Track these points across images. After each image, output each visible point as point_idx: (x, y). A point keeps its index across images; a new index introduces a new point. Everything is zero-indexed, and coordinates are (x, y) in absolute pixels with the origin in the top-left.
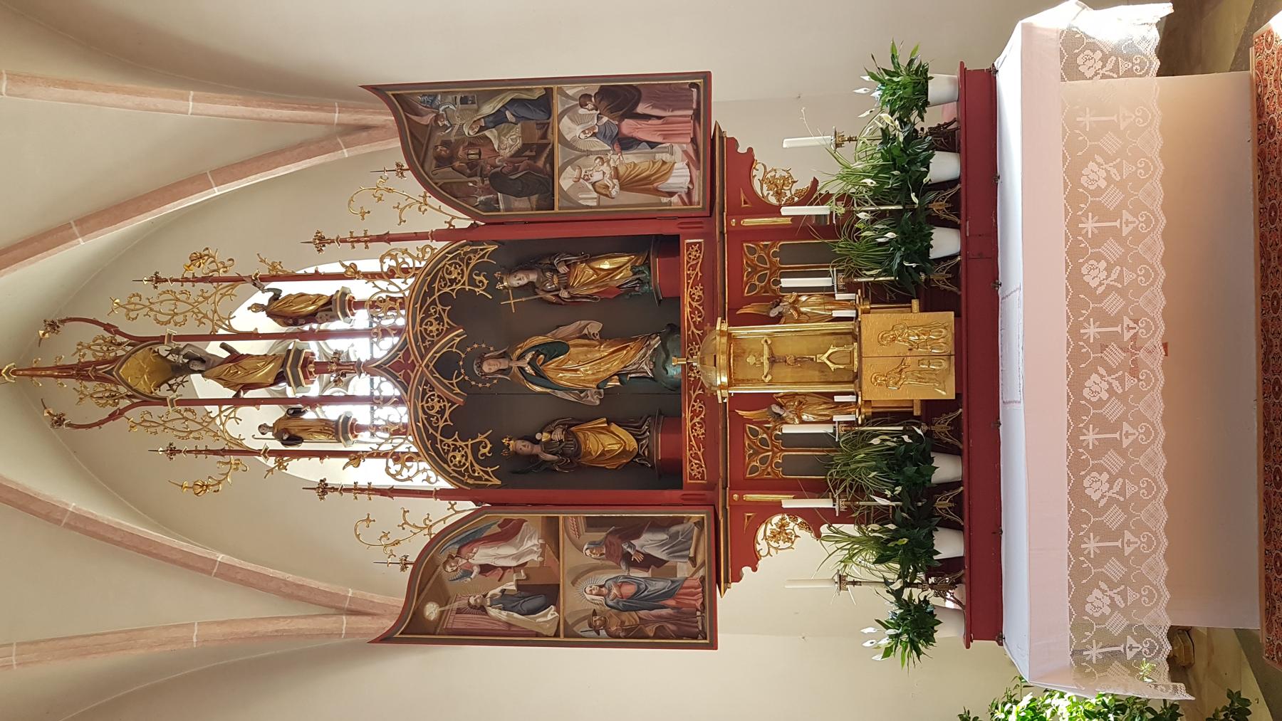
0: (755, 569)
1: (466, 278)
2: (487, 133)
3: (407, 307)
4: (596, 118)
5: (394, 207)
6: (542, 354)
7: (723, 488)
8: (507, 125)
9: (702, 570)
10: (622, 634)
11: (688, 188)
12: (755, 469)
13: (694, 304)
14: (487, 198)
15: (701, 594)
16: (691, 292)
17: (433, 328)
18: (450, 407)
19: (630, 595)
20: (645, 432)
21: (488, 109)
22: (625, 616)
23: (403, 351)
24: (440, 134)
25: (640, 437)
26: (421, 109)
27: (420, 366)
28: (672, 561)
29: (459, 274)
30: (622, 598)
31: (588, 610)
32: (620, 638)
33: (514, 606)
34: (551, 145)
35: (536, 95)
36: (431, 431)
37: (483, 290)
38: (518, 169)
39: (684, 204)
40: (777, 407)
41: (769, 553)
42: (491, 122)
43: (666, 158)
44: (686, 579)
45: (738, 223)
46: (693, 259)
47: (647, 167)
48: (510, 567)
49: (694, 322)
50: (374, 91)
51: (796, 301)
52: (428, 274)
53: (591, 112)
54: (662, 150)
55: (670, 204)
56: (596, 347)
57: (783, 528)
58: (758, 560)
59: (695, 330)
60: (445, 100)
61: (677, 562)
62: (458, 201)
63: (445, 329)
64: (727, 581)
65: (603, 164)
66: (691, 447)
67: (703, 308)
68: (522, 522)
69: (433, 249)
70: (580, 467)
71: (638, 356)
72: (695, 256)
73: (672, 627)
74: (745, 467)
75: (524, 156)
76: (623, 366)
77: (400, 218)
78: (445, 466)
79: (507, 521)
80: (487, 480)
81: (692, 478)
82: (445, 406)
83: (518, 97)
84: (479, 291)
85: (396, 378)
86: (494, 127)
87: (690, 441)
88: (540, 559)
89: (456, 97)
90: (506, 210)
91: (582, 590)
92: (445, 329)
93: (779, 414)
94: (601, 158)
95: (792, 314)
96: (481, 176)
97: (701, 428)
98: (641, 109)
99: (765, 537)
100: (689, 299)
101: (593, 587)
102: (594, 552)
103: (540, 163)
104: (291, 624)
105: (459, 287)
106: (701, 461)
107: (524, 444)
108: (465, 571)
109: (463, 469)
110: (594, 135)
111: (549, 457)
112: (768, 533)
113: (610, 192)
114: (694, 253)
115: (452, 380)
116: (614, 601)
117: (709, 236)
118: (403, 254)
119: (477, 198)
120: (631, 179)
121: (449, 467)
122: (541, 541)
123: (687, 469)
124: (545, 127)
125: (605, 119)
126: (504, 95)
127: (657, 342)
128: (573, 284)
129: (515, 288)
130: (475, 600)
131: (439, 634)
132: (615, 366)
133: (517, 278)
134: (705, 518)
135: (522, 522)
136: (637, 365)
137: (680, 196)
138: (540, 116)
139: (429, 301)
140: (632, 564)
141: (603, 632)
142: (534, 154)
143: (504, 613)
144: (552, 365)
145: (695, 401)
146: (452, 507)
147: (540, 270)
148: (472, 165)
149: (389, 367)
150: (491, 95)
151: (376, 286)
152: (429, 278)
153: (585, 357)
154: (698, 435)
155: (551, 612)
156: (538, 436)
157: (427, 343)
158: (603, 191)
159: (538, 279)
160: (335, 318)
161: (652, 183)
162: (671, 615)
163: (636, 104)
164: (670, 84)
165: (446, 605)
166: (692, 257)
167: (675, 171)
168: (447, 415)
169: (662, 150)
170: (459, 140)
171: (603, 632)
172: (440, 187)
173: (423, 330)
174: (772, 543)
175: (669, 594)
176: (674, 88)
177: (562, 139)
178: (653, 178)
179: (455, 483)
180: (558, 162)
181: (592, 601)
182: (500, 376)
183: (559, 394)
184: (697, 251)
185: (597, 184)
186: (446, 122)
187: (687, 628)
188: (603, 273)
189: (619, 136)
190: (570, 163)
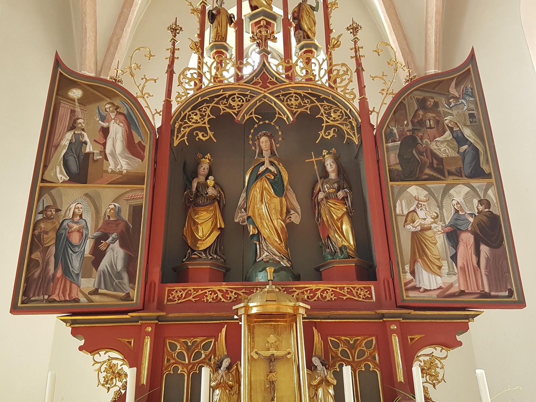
0: (81, 348)
1: (331, 123)
2: (448, 132)
3: (307, 82)
4: (471, 212)
5: (383, 73)
6: (275, 178)
7: (159, 316)
8: (457, 146)
9: (86, 300)
10: (36, 232)
11: (420, 288)
12: (173, 347)
13: (319, 293)
14: (395, 134)
15: (63, 299)
16: (329, 290)
17: (293, 102)
18: (234, 113)
19: (70, 240)
20: (211, 256)
21: (467, 133)
22: (53, 235)
23: (276, 81)
24: (443, 100)
25: (207, 252)
26: (461, 87)
27: (265, 92)
28: (96, 274)
29: (334, 118)
30: (68, 233)
31: (62, 205)
32: (34, 229)
33: (72, 150)
34: (444, 179)
35: (484, 167)
36: (216, 99)
37: (323, 136)
38: (422, 155)
39: (406, 284)
40: (227, 364)
41: (97, 362)
42: (457, 135)
43: (444, 269)
44: (79, 286)
45: (394, 331)
46: (357, 293)
47: (434, 253)
48: (105, 148)
49: (303, 293)
50: (471, 55)
51: (328, 383)
52: (333, 97)
53: (476, 209)
54: (450, 266)
55: (405, 272)
56: (281, 216)
57: (117, 375)
58: (90, 353)
59: (296, 293)
60: (470, 103)
61: (95, 278)
62: (391, 114)
63: (293, 109)
64: (74, 322)
65: (432, 218)
66: (196, 290)
67: (315, 300)
68: (142, 159)
69: (353, 99)
70: (187, 209)
71: (274, 250)
72: (360, 294)
73: (37, 274)
74: (177, 338)
75: (432, 160)
76: (265, 237)
77: (376, 77)
78: (189, 109)
79: (143, 148)
80: (177, 136)
81: (170, 291)
82: (235, 109)
83: (480, 153)
84: (322, 133)
85: (256, 76)
86: (453, 137)
87: (202, 290)
88: (110, 171)
89: (474, 110)
90: (387, 148)
91: (79, 201)
92: (293, 109)
93: (221, 366)
94: (437, 216)
95: (316, 379)
96: (413, 129)
97: (213, 298)
98: (484, 249)
99: (111, 359)
100: (322, 288)
101: (81, 210)
102: (112, 211)
103: (427, 171)
104: (90, 39)
105: (325, 119)
106: (184, 299)
107: (206, 169)
108: (105, 117)
109: (186, 120)
110: (457, 211)
111: (195, 185)
112: (114, 362)
113: (410, 224)
114: (362, 293)
115: (254, 114)
116: (67, 227)
117: (379, 304)
118: (348, 79)
119: (395, 127)
120: (422, 240)
121: (189, 112)
122: (125, 171)
123: (178, 287)
124: (459, 174)
125: (471, 220)
126: (481, 144)
127: (285, 264)
128: (329, 202)
129: (324, 163)
130: (80, 123)
131: (56, 98)
132: (265, 232)
133: (332, 164)
134: (132, 302)
135: (142, 159)
136: (266, 249)
137: (412, 280)
138: (467, 170)
139: (314, 99)
140: (98, 241)
141: (40, 217)
142: (435, 166)
143: (67, 143)
144: (267, 185)
145: (235, 294)
146: (157, 112)
147: (339, 180)
148: (422, 123)
149: (264, 72)
150: (479, 134)
151: (324, 61)
152: (330, 98)
153: (273, 208)
154: (207, 296)
155: (63, 177)
156: (211, 178)
157: (282, 98)
158: (409, 218)
159: (331, 179)
160: (298, 41)
161: (420, 257)
162: (48, 273)
163: (487, 244)
164: (509, 273)
165: (79, 103)
166: (359, 292)
167: (433, 276)
168: (228, 110)
169: (450, 266)
170: (440, 113)
171: (40, 217)
172: (401, 102)
173: (291, 95)
174: (105, 366)
175: (67, 272)
176: (506, 276)
177: (448, 188)
178: (425, 258)
179: (176, 114)
180: (431, 185)
181: (69, 209)
182: (257, 151)
183: (244, 195)
184: (365, 295)
185: (415, 214)
186: (453, 104)
187: (34, 286)
188: (339, 224)
189: (458, 231)
190: (431, 193)
